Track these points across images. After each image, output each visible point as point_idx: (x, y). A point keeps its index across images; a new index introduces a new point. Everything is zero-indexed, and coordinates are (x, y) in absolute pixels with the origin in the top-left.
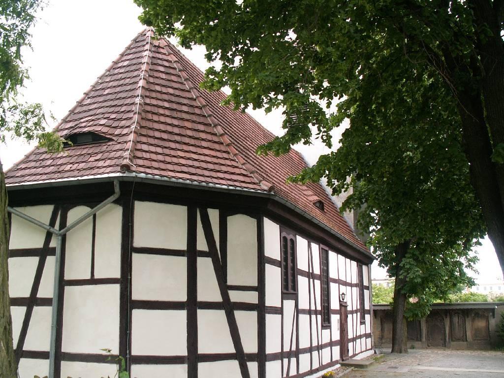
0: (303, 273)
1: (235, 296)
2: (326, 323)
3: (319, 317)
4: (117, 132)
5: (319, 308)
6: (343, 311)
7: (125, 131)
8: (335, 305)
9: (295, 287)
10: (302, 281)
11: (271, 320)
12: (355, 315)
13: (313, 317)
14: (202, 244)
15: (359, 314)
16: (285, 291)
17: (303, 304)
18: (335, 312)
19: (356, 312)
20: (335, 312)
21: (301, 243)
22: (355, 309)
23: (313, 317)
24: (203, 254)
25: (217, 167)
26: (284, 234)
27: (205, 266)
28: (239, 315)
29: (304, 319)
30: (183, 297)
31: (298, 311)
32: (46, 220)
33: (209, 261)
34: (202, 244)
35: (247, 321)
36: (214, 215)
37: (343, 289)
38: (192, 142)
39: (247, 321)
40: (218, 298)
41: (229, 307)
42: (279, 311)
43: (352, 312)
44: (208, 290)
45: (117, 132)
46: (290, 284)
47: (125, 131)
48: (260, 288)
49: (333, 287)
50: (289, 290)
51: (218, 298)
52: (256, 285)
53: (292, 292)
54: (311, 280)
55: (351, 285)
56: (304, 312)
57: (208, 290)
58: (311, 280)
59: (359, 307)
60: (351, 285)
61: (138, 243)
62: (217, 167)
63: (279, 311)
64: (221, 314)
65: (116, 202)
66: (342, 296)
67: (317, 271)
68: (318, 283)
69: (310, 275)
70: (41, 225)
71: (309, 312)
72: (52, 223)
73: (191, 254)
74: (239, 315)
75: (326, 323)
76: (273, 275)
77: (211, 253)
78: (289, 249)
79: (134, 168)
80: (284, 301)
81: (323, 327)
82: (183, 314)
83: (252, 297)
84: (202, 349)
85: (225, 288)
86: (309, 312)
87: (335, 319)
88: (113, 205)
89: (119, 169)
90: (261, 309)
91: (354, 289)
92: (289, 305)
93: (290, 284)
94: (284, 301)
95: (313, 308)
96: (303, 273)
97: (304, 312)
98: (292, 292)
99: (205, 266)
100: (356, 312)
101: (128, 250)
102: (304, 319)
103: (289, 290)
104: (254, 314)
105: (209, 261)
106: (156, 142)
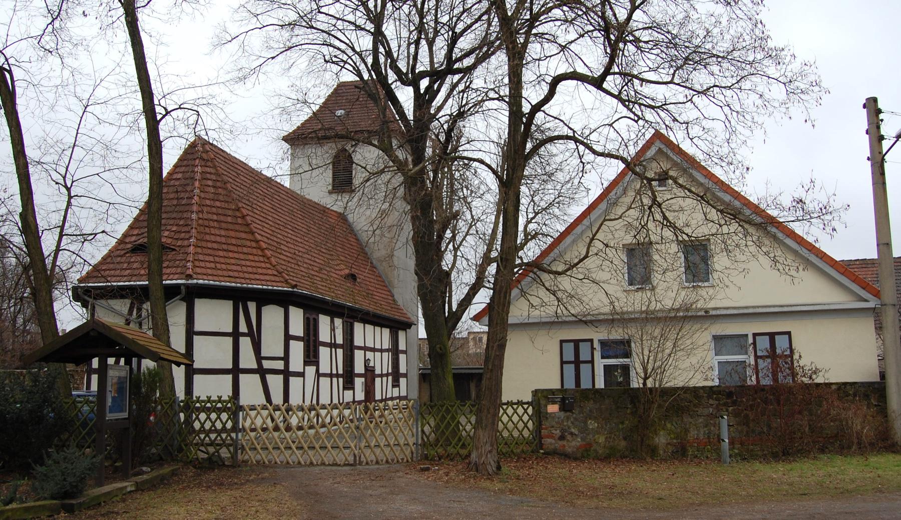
0: (325, 344)
1: (267, 364)
2: (349, 384)
3: (341, 380)
4: (179, 243)
5: (341, 372)
6: (370, 374)
7: (186, 243)
8: (359, 368)
9: (316, 355)
10: (324, 352)
11: (294, 382)
12: (385, 379)
13: (335, 380)
14: (243, 328)
15: (390, 378)
16: (307, 360)
17: (325, 368)
18: (359, 375)
19: (387, 375)
20: (359, 375)
21: (324, 321)
22: (385, 372)
23: (335, 380)
24: (244, 335)
25: (254, 270)
26: (307, 315)
27: (245, 343)
28: (269, 377)
29: (325, 382)
30: (230, 330)
31: (318, 375)
32: (125, 310)
33: (248, 339)
34: (243, 328)
35: (275, 382)
36: (252, 307)
37: (370, 355)
38: (235, 249)
39: (275, 382)
40: (255, 366)
41: (262, 372)
42: (302, 375)
43: (381, 376)
44: (248, 360)
45: (179, 243)
46: (312, 354)
47: (186, 243)
48: (286, 358)
49: (359, 356)
50: (311, 358)
51: (255, 366)
52: (283, 356)
53: (314, 360)
54: (333, 350)
55: (381, 351)
56: (325, 375)
57: (248, 360)
58: (333, 350)
59: (390, 371)
60: (381, 351)
61: (198, 327)
62: (254, 270)
63: (302, 375)
64: (256, 377)
65: (182, 299)
66: (366, 361)
67: (340, 340)
68: (340, 352)
69: (333, 345)
70: (121, 315)
71: (331, 375)
72: (130, 312)
73: (236, 335)
74: (269, 377)
75: (349, 384)
76: (297, 350)
77: (250, 334)
78: (311, 328)
79: (195, 276)
80: (306, 367)
81: (345, 388)
82: (229, 377)
83: (280, 365)
84: (229, 377)
85: (259, 358)
86: (331, 375)
87: (359, 382)
88: (178, 301)
89: (184, 276)
90: (287, 374)
91: (385, 355)
92: (311, 371)
93: (312, 354)
94: (306, 367)
95: (334, 372)
96: (325, 344)
97: (325, 375)
98: (314, 360)
99: (245, 343)
100: (387, 375)
101: (191, 333)
102: (325, 382)
103: (311, 358)
104: (280, 377)
105: (248, 339)
106: (209, 251)
